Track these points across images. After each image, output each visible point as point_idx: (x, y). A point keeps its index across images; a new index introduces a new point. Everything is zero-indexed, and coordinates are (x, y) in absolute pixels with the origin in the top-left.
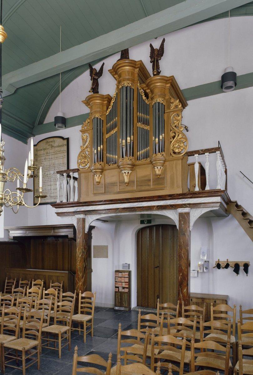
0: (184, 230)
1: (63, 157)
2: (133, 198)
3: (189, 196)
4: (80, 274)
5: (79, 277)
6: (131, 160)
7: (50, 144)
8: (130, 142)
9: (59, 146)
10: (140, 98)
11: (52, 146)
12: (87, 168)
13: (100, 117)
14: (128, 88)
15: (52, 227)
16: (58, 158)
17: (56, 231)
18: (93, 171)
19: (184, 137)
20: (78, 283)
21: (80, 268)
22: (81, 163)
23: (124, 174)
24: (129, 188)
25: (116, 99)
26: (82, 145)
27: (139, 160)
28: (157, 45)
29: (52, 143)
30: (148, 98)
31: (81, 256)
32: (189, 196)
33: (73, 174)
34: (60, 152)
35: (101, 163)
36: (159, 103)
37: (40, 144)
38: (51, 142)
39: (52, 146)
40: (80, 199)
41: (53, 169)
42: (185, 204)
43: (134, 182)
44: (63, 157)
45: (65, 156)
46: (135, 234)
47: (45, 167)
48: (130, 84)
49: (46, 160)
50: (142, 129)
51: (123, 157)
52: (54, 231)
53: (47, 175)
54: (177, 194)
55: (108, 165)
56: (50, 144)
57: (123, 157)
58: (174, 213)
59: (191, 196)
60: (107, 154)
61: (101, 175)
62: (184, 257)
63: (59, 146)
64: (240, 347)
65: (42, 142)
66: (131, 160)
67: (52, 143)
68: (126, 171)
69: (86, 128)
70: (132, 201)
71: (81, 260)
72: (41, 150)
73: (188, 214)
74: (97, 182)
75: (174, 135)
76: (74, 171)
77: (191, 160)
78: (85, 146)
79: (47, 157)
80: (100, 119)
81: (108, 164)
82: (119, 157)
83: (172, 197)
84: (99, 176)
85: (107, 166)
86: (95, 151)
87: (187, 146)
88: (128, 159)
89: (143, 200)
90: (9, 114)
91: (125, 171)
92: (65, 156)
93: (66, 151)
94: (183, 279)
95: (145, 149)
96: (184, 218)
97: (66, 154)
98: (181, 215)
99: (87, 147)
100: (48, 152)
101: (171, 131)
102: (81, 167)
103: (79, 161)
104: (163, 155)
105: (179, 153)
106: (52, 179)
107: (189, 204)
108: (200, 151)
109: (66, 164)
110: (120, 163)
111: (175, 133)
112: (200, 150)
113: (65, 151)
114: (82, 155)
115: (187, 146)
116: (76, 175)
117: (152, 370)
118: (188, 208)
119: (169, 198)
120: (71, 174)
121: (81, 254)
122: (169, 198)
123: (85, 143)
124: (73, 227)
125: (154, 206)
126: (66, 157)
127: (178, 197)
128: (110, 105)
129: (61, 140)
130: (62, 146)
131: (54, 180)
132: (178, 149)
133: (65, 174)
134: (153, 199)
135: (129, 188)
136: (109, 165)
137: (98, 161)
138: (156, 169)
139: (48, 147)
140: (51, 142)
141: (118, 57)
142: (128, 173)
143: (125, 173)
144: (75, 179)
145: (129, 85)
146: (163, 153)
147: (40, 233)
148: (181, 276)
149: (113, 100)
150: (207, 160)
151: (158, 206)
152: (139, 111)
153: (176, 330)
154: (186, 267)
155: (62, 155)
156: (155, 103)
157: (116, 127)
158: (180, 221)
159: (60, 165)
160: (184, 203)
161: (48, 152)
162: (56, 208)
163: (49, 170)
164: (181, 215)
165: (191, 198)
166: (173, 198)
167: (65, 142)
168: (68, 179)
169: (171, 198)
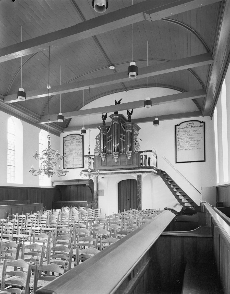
7: (73, 137)
9: (78, 139)
11: (74, 139)
17: (79, 182)
24: (117, 164)
26: (96, 145)
28: (130, 111)
29: (74, 137)
30: (125, 129)
37: (67, 137)
38: (74, 136)
39: (74, 139)
42: (139, 172)
43: (119, 162)
53: (71, 153)
63: (78, 139)
65: (68, 136)
67: (74, 137)
68: (116, 158)
72: (68, 140)
73: (141, 175)
77: (142, 154)
78: (97, 145)
79: (71, 144)
83: (134, 169)
86: (103, 148)
90: (219, 221)
96: (139, 177)
98: (138, 175)
99: (98, 146)
102: (95, 154)
105: (138, 151)
109: (82, 148)
116: (93, 157)
117: (162, 233)
125: (127, 172)
130: (80, 139)
133: (88, 157)
135: (117, 164)
137: (104, 153)
139: (72, 139)
140: (74, 136)
141: (113, 113)
146: (131, 151)
150: (149, 155)
153: (14, 267)
155: (79, 144)
158: (138, 178)
160: (139, 171)
164: (138, 175)
168: (90, 159)
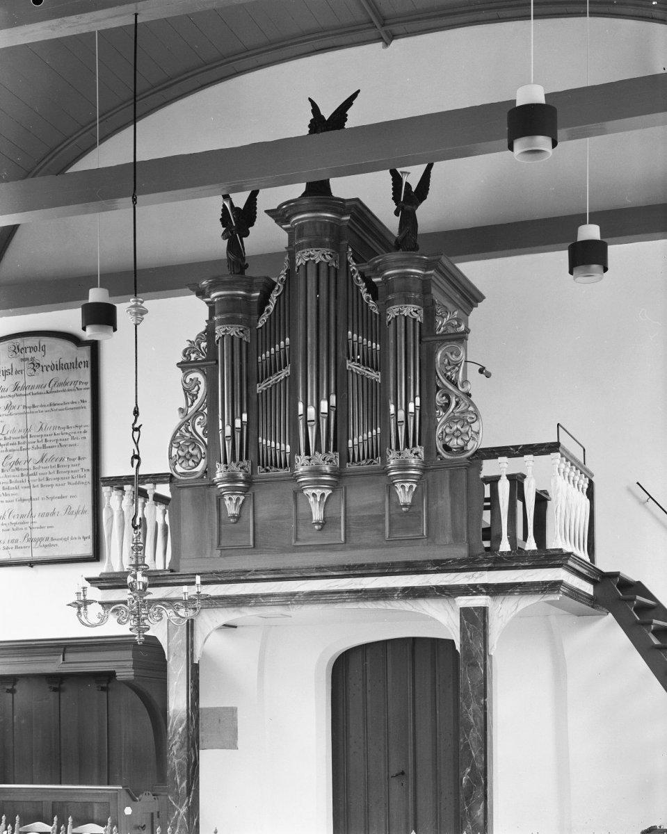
0: (474, 654)
1: (74, 406)
2: (23, 333)
3: (485, 565)
4: (181, 783)
5: (177, 793)
6: (331, 461)
8: (326, 411)
9: (60, 367)
10: (355, 293)
12: (198, 475)
13: (241, 334)
14: (323, 269)
15: (58, 646)
16: (55, 407)
18: (219, 486)
19: (471, 409)
20: (174, 809)
21: (180, 764)
22: (180, 457)
23: (311, 499)
24: (326, 539)
25: (284, 286)
26: (183, 406)
27: (354, 460)
30: (375, 298)
31: (183, 729)
32: (485, 565)
33: (155, 488)
34: (66, 388)
35: (245, 462)
36: (406, 318)
40: (178, 563)
41: (40, 445)
42: (474, 586)
44: (74, 406)
45: (83, 401)
46: (328, 664)
47: (8, 436)
48: (328, 258)
49: (13, 411)
50: (360, 377)
51: (308, 453)
52: (64, 660)
54: (454, 560)
55: (263, 470)
56: (29, 355)
57: (308, 453)
58: (449, 609)
59: (489, 565)
60: (260, 439)
61: (242, 498)
62: (476, 724)
64: (136, 6)
66: (331, 461)
68: (318, 492)
69: (193, 356)
70: (335, 573)
71: (182, 744)
73: (484, 611)
74: (233, 516)
75: (447, 401)
76: (157, 478)
77: (489, 468)
80: (241, 339)
81: (263, 467)
82: (296, 450)
83: (442, 566)
84: (238, 499)
85: (260, 472)
87: (481, 434)
88: (324, 460)
89: (364, 572)
91: (314, 491)
92: (83, 401)
93: (89, 385)
94: (475, 783)
95: (370, 433)
96: (475, 621)
97: (87, 395)
98: (465, 612)
99: (197, 413)
100: (21, 385)
101: (438, 391)
102: (179, 469)
103: (175, 451)
104: (416, 454)
105: (462, 450)
106: (35, 478)
107: (486, 586)
108: (512, 449)
109: (89, 429)
110: (301, 469)
111: (448, 398)
112: (512, 447)
113: (84, 386)
114: (183, 436)
115: (478, 433)
116: (164, 490)
118: (485, 597)
119: (435, 568)
120: (147, 487)
121: (184, 724)
122: (435, 568)
123: (193, 401)
124: (131, 646)
125: (394, 590)
126: (88, 405)
127: (457, 567)
128: (268, 303)
129: (69, 346)
130: (75, 365)
131: (45, 483)
132: (456, 440)
133: (127, 488)
134: (391, 570)
135: (326, 539)
136: (267, 471)
138: (399, 491)
142: (323, 495)
143: (314, 495)
144: (159, 499)
145: (323, 259)
147: (11, 664)
148: (469, 774)
149: (276, 288)
151: (405, 589)
152: (350, 327)
154: (480, 751)
156: (396, 316)
157: (285, 365)
159: (67, 431)
161: (21, 385)
162: (101, 588)
163: (24, 446)
164: (465, 612)
165: (490, 569)
166: (443, 568)
167: (84, 354)
168: (141, 500)
169: (440, 568)
